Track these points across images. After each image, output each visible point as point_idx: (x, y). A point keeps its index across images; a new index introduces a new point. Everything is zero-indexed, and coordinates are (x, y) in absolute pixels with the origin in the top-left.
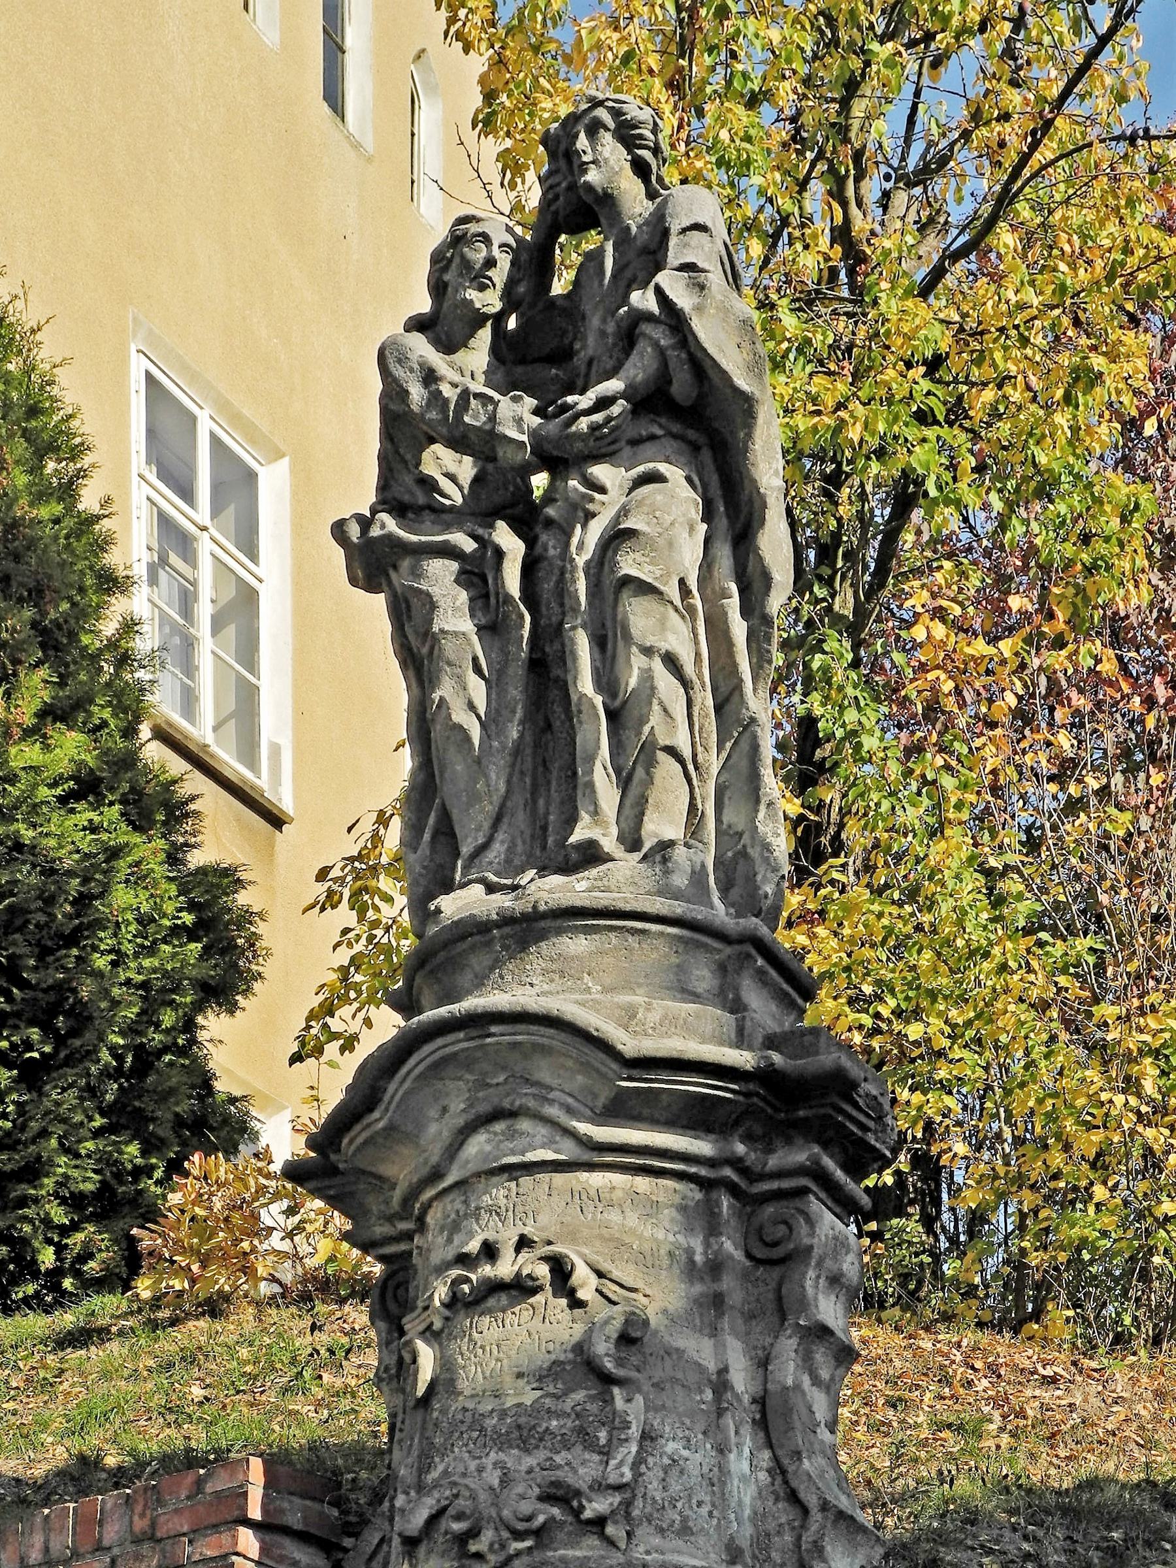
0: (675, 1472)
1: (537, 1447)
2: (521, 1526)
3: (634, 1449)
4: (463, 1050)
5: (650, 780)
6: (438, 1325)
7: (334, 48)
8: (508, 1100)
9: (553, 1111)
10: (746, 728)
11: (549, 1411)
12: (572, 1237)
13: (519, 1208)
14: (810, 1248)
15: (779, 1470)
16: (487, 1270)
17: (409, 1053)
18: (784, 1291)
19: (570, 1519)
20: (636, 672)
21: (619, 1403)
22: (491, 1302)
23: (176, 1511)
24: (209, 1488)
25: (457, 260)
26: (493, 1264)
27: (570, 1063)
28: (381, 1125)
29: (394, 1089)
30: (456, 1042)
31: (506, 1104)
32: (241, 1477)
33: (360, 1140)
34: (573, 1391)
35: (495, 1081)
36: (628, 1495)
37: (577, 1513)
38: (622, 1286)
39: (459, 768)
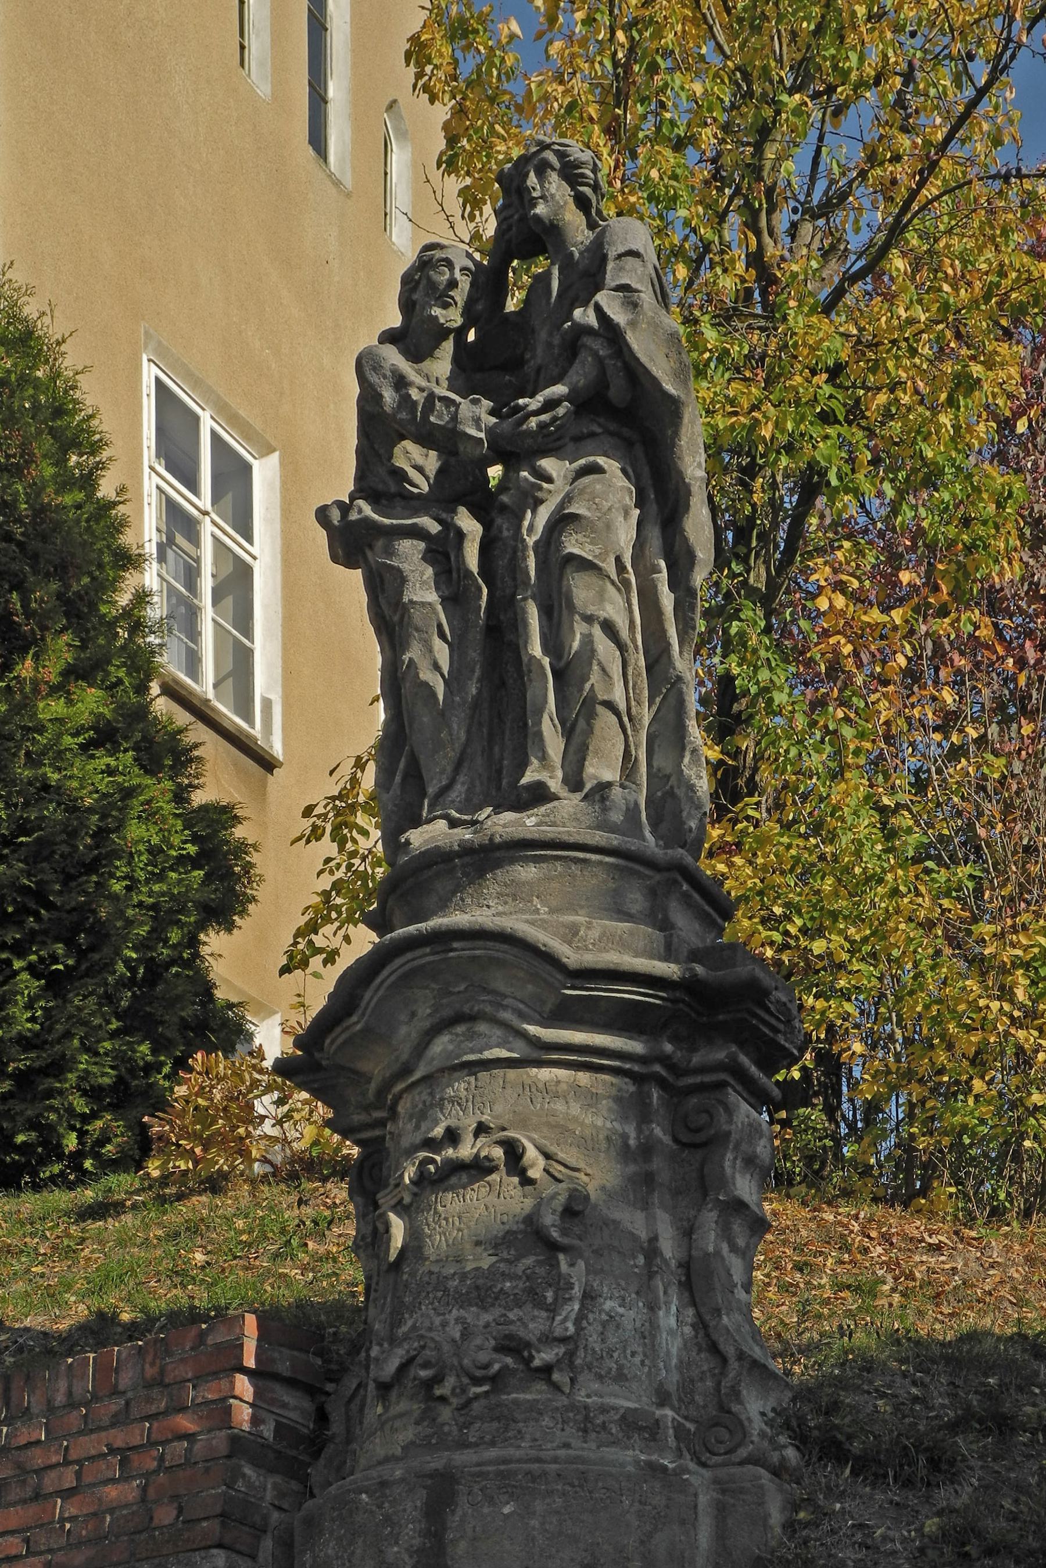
0: (611, 1327)
1: (493, 1305)
2: (479, 1373)
3: (577, 1307)
4: (429, 963)
5: (590, 730)
9: (506, 1015)
10: (673, 685)
11: (503, 1274)
12: (523, 1124)
13: (478, 1099)
14: (729, 1133)
15: (701, 1325)
17: (383, 966)
18: (706, 1170)
19: (521, 1367)
20: (578, 637)
21: (564, 1267)
22: (454, 1180)
24: (210, 1340)
28: (358, 1027)
30: (425, 956)
31: (466, 1009)
35: (457, 989)
36: (571, 1346)
39: (425, 719)
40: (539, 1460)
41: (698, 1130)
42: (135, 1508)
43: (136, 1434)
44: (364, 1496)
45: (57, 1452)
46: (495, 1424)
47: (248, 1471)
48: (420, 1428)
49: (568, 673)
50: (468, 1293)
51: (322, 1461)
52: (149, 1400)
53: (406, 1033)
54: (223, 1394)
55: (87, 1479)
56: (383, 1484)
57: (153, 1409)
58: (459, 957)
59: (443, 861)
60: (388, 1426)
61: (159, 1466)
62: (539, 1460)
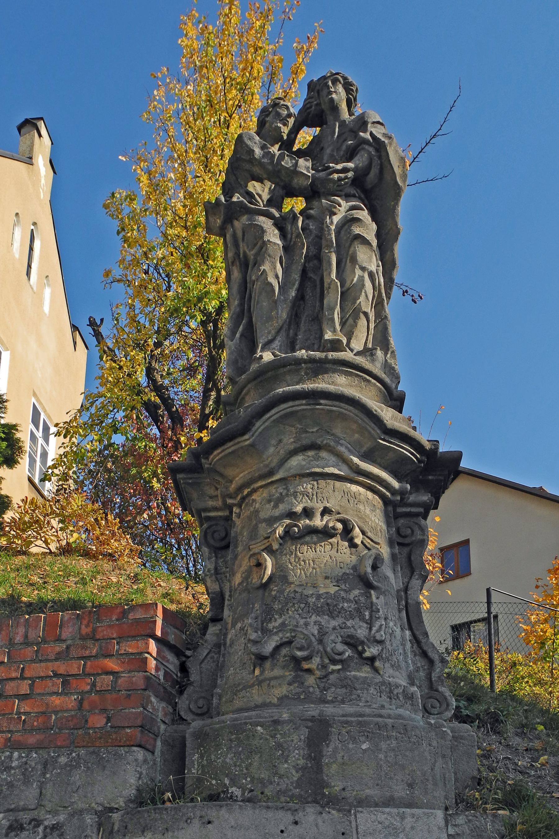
1: (338, 616)
2: (337, 657)
4: (303, 410)
5: (355, 325)
6: (275, 546)
7: (29, 266)
8: (320, 439)
9: (342, 449)
10: (382, 319)
11: (343, 598)
13: (319, 495)
16: (305, 522)
18: (412, 558)
19: (356, 656)
20: (357, 276)
22: (308, 539)
23: (110, 626)
24: (131, 616)
25: (273, 113)
26: (310, 520)
27: (354, 427)
28: (247, 443)
29: (259, 426)
30: (300, 405)
31: (319, 442)
32: (152, 612)
33: (230, 450)
34: (354, 589)
35: (311, 430)
37: (360, 654)
38: (372, 540)
39: (265, 304)
40: (381, 716)
41: (405, 537)
42: (73, 713)
43: (75, 667)
44: (259, 728)
45: (16, 671)
46: (344, 690)
47: (153, 699)
48: (292, 687)
49: (349, 295)
50: (322, 607)
51: (185, 695)
52: (84, 648)
53: (272, 455)
54: (139, 651)
55: (38, 691)
56: (276, 722)
57: (87, 653)
58: (322, 409)
59: (294, 364)
60: (265, 685)
61: (91, 689)
62: (381, 716)
